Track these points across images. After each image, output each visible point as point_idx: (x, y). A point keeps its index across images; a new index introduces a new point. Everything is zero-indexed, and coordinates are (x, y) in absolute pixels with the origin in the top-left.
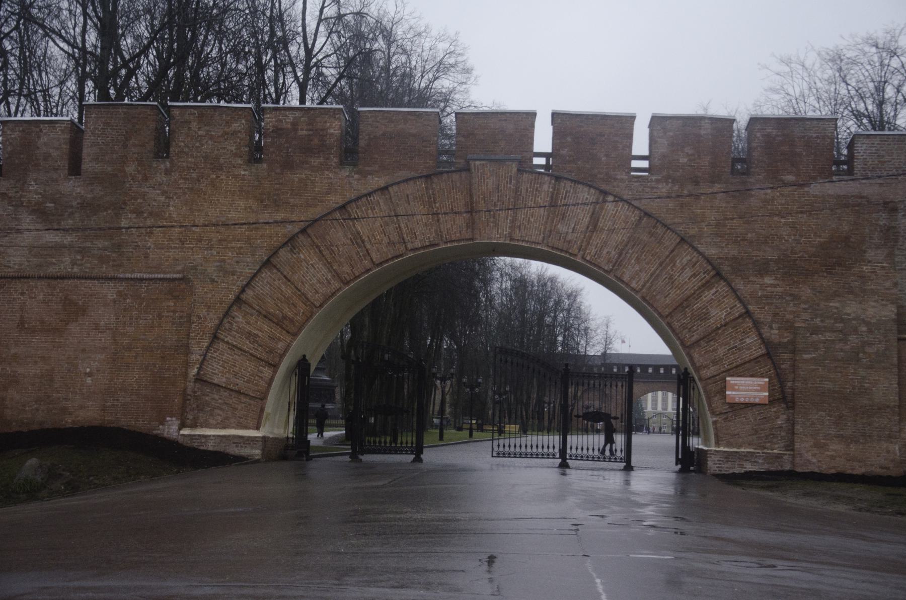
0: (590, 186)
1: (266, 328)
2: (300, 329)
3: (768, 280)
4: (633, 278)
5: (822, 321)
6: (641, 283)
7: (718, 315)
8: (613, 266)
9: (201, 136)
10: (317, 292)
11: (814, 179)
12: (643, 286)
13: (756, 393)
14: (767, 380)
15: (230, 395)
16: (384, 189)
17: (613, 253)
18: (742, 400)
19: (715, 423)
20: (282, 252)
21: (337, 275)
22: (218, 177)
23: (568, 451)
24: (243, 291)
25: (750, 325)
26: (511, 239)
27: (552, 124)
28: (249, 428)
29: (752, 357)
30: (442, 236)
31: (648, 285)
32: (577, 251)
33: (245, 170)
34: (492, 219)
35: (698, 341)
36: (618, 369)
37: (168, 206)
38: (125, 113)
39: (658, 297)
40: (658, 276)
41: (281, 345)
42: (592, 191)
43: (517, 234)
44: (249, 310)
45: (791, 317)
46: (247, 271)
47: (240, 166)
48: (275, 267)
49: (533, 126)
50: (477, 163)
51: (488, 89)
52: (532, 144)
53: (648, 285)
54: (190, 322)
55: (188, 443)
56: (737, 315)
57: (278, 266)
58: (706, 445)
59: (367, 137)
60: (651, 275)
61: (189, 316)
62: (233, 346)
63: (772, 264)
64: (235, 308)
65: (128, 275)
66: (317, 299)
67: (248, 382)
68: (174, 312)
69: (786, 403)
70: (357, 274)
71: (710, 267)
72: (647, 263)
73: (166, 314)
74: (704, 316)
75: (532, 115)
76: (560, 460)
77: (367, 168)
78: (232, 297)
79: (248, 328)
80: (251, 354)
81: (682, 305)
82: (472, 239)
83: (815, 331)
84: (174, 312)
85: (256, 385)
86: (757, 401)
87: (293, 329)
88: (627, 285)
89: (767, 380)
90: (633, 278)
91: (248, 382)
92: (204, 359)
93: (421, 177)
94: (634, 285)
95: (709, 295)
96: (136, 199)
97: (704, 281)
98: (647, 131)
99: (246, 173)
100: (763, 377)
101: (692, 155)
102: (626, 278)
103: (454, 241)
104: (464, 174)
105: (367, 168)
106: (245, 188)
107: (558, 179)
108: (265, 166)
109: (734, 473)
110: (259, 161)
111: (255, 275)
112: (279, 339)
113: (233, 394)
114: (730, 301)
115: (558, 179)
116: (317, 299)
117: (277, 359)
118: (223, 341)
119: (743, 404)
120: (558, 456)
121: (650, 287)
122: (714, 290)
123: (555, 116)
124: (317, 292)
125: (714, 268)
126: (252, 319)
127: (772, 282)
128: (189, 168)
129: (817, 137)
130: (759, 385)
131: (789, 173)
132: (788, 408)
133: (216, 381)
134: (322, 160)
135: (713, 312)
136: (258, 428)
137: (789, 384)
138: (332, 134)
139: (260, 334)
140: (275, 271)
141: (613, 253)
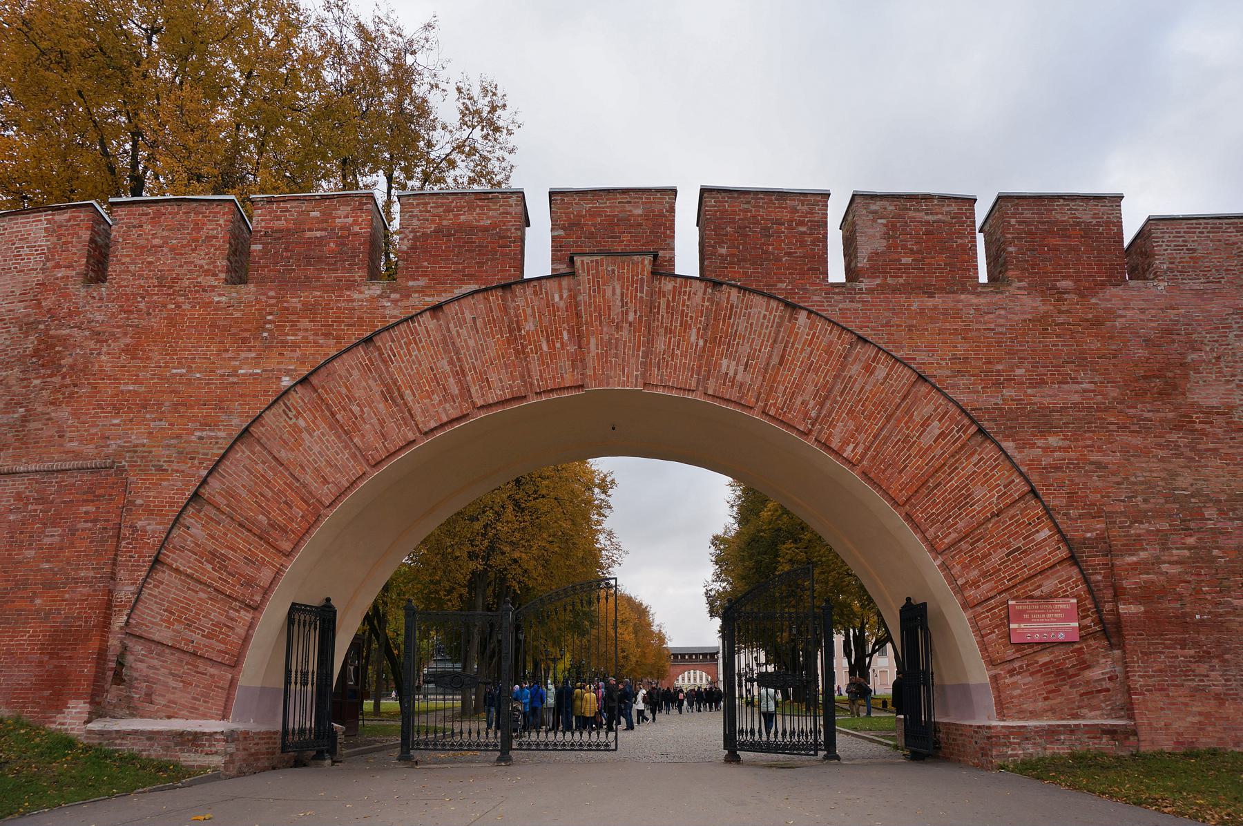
0: (771, 297)
1: (241, 545)
2: (296, 546)
3: (1053, 441)
4: (845, 443)
5: (1145, 501)
6: (860, 450)
7: (985, 496)
11: (1103, 285)
12: (863, 456)
13: (1059, 625)
14: (1075, 601)
15: (180, 660)
16: (436, 309)
20: (269, 417)
21: (359, 453)
25: (1040, 511)
29: (1046, 565)
30: (531, 384)
33: (220, 295)
35: (955, 543)
36: (1024, 587)
38: (49, 221)
40: (886, 439)
41: (266, 575)
42: (773, 304)
43: (655, 376)
44: (212, 512)
46: (215, 451)
48: (258, 441)
49: (672, 210)
56: (1016, 496)
57: (264, 440)
58: (1001, 716)
60: (876, 437)
62: (188, 576)
63: (1056, 415)
64: (191, 510)
65: (32, 467)
66: (325, 493)
68: (95, 521)
69: (1108, 639)
71: (966, 421)
72: (868, 418)
73: (82, 525)
74: (963, 500)
77: (411, 283)
78: (188, 494)
79: (211, 545)
80: (216, 590)
81: (921, 486)
82: (582, 386)
83: (1138, 517)
84: (95, 521)
85: (223, 642)
86: (1061, 637)
87: (286, 546)
88: (837, 454)
89: (1075, 601)
90: (845, 443)
92: (137, 600)
94: (848, 453)
95: (968, 466)
96: (53, 347)
97: (958, 444)
101: (919, 252)
102: (835, 444)
103: (552, 390)
105: (411, 283)
106: (219, 323)
109: (895, 684)
111: (223, 457)
112: (263, 563)
113: (187, 658)
114: (1002, 474)
116: (325, 493)
117: (258, 598)
118: (170, 566)
121: (874, 458)
122: (975, 458)
123: (705, 192)
124: (325, 481)
125: (973, 421)
126: (218, 531)
127: (1061, 443)
128: (135, 295)
129: (1098, 224)
131: (1065, 278)
132: (1112, 647)
133: (157, 637)
135: (979, 492)
136: (224, 717)
137: (1108, 606)
138: (356, 234)
139: (230, 554)
140: (258, 448)
141: (812, 403)
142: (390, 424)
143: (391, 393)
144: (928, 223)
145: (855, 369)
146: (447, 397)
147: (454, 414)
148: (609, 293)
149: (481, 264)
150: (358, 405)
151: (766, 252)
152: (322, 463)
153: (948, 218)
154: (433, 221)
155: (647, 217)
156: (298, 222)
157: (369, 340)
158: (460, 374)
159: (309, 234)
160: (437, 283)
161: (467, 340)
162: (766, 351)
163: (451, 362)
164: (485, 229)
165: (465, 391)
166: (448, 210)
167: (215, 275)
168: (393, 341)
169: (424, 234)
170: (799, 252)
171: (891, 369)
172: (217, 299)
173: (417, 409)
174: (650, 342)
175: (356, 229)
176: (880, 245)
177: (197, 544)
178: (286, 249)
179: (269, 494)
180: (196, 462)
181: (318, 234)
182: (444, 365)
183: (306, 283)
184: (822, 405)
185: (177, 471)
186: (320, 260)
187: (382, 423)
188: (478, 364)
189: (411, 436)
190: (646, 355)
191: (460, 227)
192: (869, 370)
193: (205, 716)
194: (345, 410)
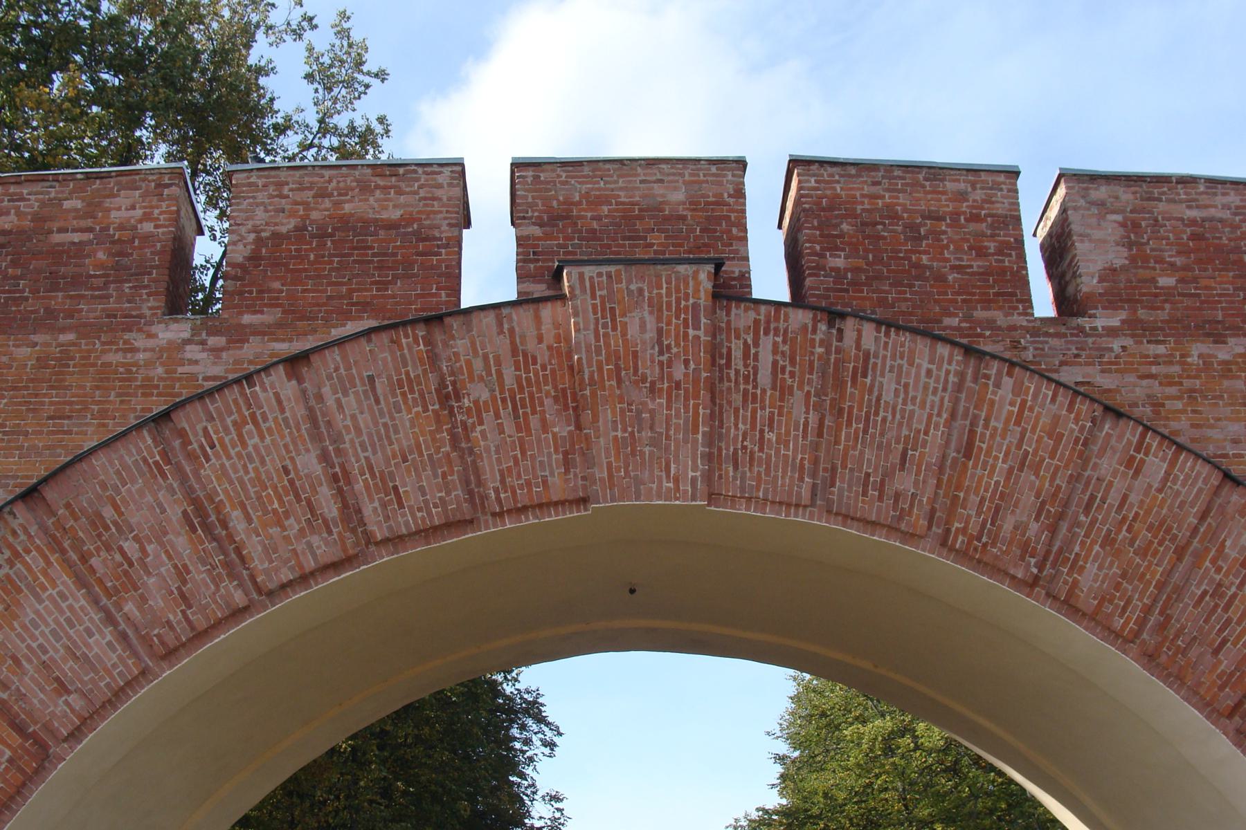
8: (1041, 567)
10: (62, 688)
12: (1142, 623)
17: (1034, 526)
26: (712, 497)
28: (1176, 677)
31: (1153, 619)
32: (923, 523)
34: (646, 434)
39: (1193, 654)
42: (943, 350)
53: (1153, 619)
59: (252, 236)
70: (201, 622)
77: (247, 319)
93: (138, 427)
103: (524, 509)
105: (247, 319)
107: (834, 316)
115: (834, 316)
134: (348, 208)
142: (199, 574)
143: (203, 517)
144: (1193, 222)
145: (1107, 465)
146: (316, 523)
147: (335, 554)
148: (633, 331)
149: (382, 285)
151: (917, 265)
152: (57, 652)
153: (1226, 215)
154: (293, 214)
155: (693, 204)
156: (38, 219)
157: (165, 416)
158: (340, 480)
159: (57, 238)
160: (296, 316)
161: (350, 411)
162: (936, 436)
163: (324, 457)
164: (391, 226)
165: (351, 513)
166: (323, 194)
169: (276, 236)
170: (977, 265)
171: (1172, 464)
173: (254, 547)
174: (716, 417)
175: (148, 227)
176: (1118, 257)
178: (14, 264)
181: (76, 237)
182: (309, 463)
183: (49, 321)
184: (1053, 530)
186: (77, 281)
187: (182, 573)
188: (378, 460)
189: (239, 598)
190: (710, 440)
191: (344, 223)
192: (1133, 466)
194: (109, 549)
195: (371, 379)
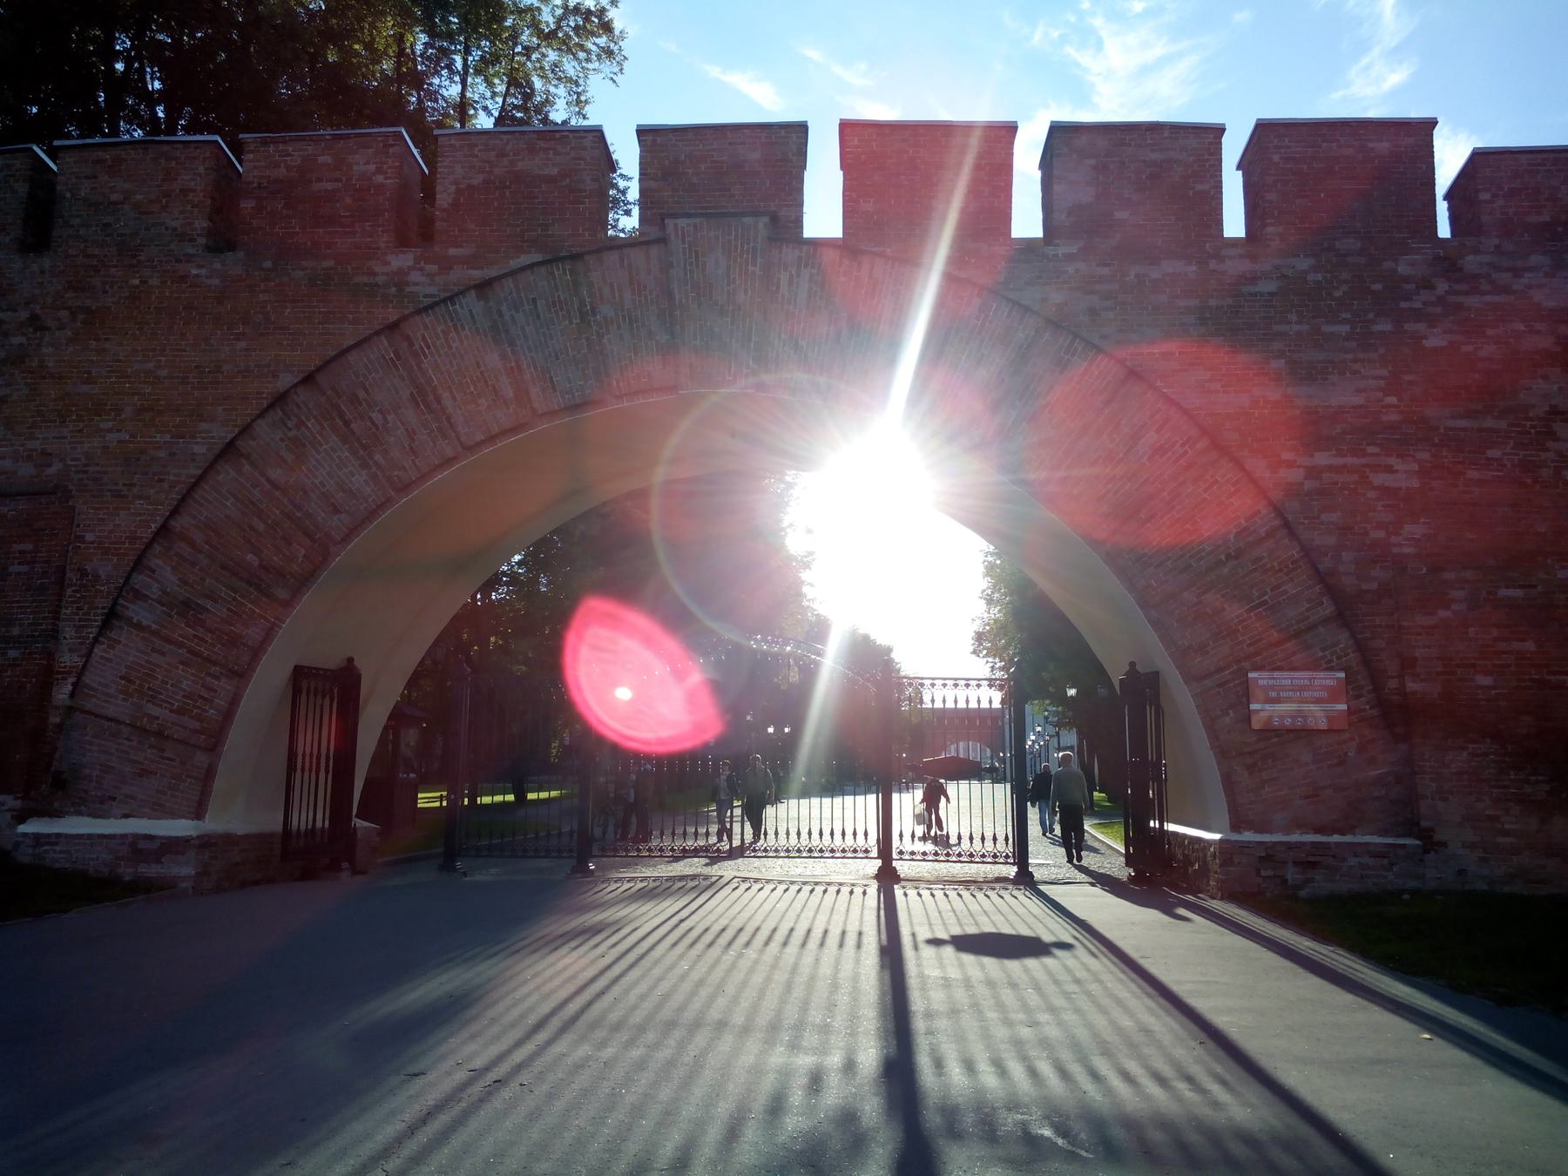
9: (115, 203)
14: (1342, 675)
18: (1288, 722)
19: (187, 130)
20: (262, 427)
22: (143, 282)
23: (896, 842)
24: (175, 512)
27: (842, 167)
33: (200, 267)
37: (39, 345)
45: (1381, 534)
47: (189, 258)
50: (682, 222)
51: (792, 552)
52: (801, 227)
54: (61, 583)
55: (25, 856)
59: (453, 188)
61: (62, 570)
67: (180, 712)
75: (801, 129)
76: (879, 863)
89: (1342, 675)
91: (180, 712)
98: (1037, 175)
99: (203, 271)
100: (1331, 669)
104: (654, 251)
108: (241, 254)
110: (231, 246)
119: (1289, 731)
120: (874, 853)
130: (1324, 688)
133: (110, 711)
134: (520, 166)
136: (199, 814)
139: (209, 605)
150: (380, 411)
164: (550, 180)
167: (192, 240)
168: (426, 327)
169: (470, 187)
172: (194, 272)
175: (380, 179)
177: (164, 592)
179: (261, 527)
180: (166, 485)
181: (329, 186)
185: (140, 497)
193: (173, 815)
195: (534, 300)
